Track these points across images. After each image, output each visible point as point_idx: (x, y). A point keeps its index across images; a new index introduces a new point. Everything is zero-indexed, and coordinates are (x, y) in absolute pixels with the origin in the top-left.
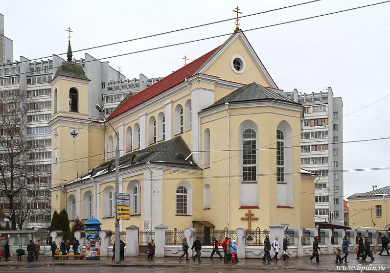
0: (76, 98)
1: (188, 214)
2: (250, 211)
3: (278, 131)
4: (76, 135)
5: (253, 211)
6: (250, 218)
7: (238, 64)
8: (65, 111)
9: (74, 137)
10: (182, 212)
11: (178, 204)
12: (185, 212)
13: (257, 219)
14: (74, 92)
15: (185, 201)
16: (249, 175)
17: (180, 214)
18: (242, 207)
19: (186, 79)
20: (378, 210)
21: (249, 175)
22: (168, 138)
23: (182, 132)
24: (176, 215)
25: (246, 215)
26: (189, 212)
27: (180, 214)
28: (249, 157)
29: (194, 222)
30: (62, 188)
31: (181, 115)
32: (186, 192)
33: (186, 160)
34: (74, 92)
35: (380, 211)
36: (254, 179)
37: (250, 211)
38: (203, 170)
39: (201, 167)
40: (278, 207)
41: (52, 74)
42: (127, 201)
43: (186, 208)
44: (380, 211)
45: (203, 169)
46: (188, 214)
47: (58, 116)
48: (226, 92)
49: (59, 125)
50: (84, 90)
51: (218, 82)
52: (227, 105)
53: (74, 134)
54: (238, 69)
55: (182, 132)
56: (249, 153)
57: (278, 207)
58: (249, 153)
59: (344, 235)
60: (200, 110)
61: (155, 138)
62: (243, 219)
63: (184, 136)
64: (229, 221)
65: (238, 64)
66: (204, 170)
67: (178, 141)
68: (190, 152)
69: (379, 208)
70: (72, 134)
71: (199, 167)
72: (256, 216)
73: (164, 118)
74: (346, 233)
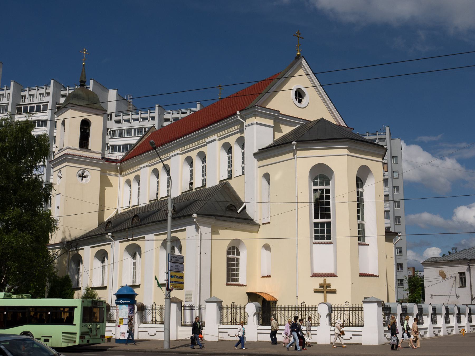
0: (88, 131)
1: (241, 282)
2: (325, 281)
3: (358, 179)
4: (85, 177)
5: (329, 280)
6: (325, 289)
7: (299, 95)
8: (74, 147)
9: (82, 180)
10: (233, 280)
11: (228, 270)
12: (237, 280)
13: (334, 292)
14: (85, 125)
15: (238, 265)
16: (323, 232)
17: (231, 283)
18: (315, 275)
19: (238, 113)
20: (461, 279)
21: (323, 232)
22: (212, 182)
23: (230, 178)
24: (227, 285)
25: (321, 286)
26: (242, 280)
27: (231, 283)
28: (322, 210)
29: (249, 294)
30: (64, 244)
31: (191, 169)
32: (238, 254)
33: (238, 212)
34: (85, 125)
35: (463, 279)
36: (329, 238)
37: (325, 281)
38: (260, 225)
39: (257, 222)
40: (361, 275)
41: (48, 102)
42: (180, 265)
43: (237, 275)
44: (463, 279)
45: (261, 224)
46: (241, 282)
47: (65, 154)
48: (287, 130)
49: (66, 164)
50: (97, 122)
51: (278, 119)
52: (294, 144)
53: (82, 176)
54: (300, 101)
55: (230, 178)
56: (322, 206)
57: (361, 275)
58: (322, 206)
59: (416, 311)
60: (256, 150)
61: (157, 194)
62: (316, 291)
63: (232, 183)
64: (292, 291)
65: (299, 95)
66: (261, 226)
67: (225, 187)
68: (242, 203)
69: (463, 277)
70: (80, 176)
71: (255, 222)
72: (332, 287)
73: (244, 144)
74: (402, 308)
